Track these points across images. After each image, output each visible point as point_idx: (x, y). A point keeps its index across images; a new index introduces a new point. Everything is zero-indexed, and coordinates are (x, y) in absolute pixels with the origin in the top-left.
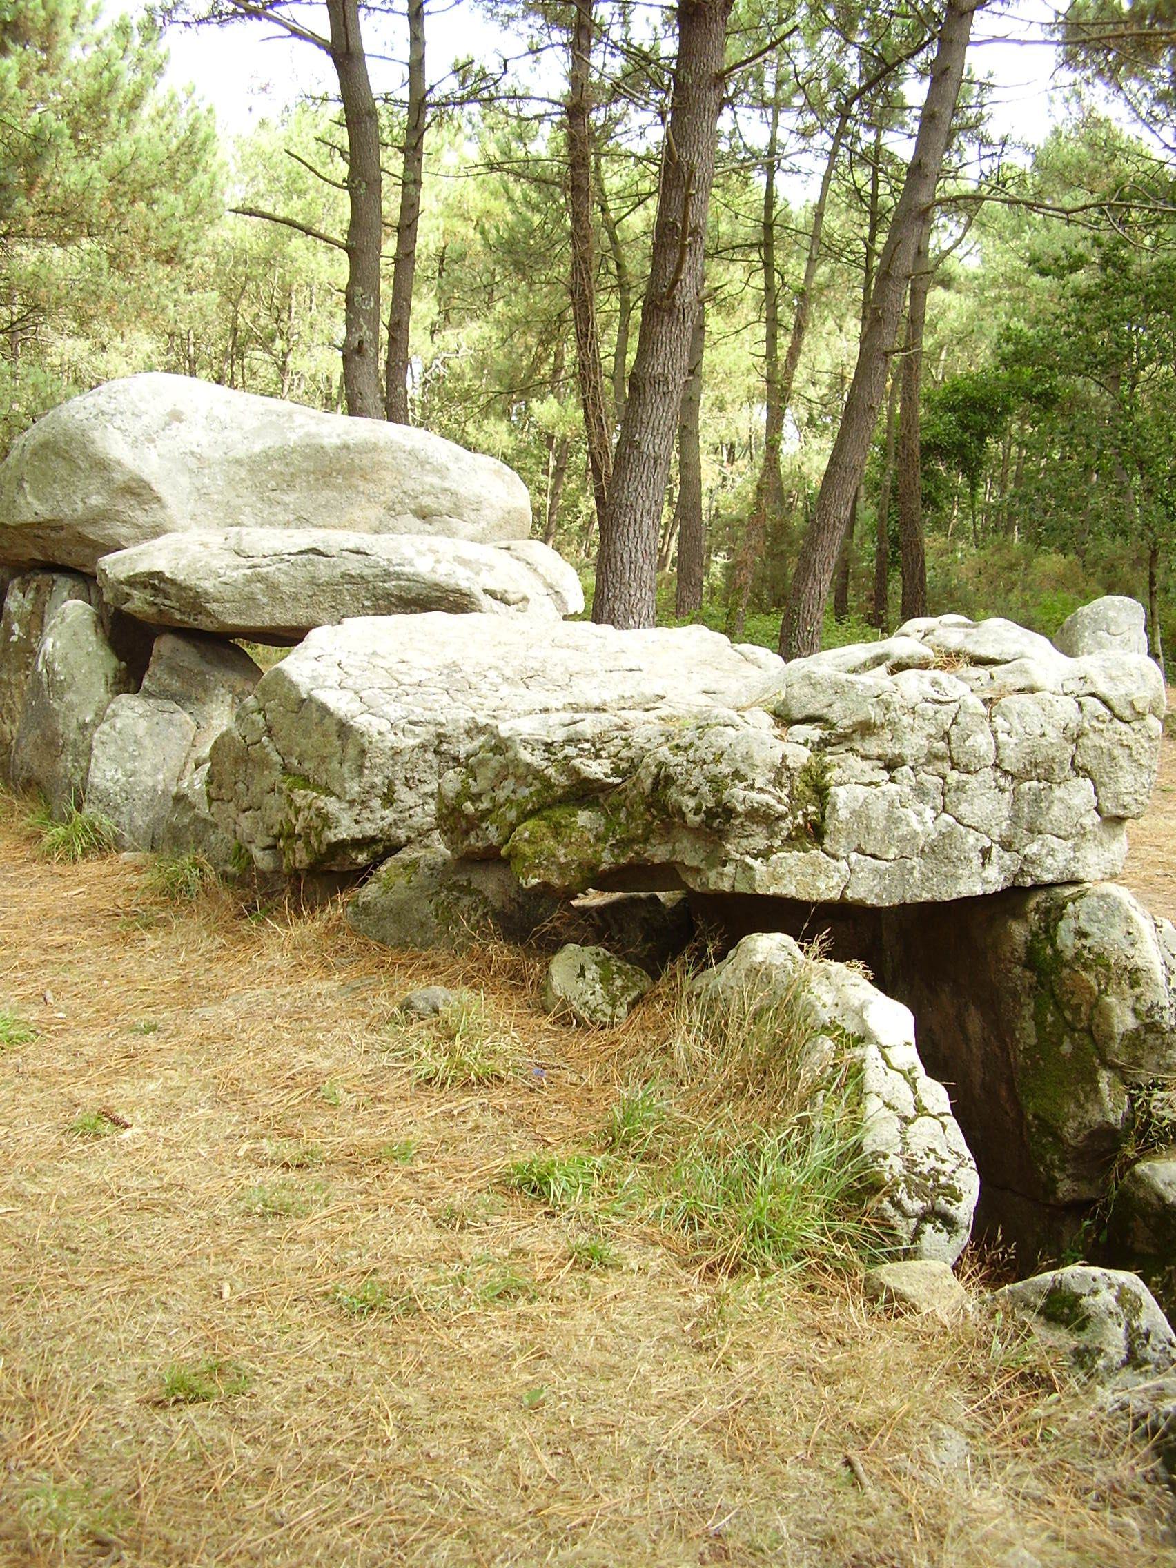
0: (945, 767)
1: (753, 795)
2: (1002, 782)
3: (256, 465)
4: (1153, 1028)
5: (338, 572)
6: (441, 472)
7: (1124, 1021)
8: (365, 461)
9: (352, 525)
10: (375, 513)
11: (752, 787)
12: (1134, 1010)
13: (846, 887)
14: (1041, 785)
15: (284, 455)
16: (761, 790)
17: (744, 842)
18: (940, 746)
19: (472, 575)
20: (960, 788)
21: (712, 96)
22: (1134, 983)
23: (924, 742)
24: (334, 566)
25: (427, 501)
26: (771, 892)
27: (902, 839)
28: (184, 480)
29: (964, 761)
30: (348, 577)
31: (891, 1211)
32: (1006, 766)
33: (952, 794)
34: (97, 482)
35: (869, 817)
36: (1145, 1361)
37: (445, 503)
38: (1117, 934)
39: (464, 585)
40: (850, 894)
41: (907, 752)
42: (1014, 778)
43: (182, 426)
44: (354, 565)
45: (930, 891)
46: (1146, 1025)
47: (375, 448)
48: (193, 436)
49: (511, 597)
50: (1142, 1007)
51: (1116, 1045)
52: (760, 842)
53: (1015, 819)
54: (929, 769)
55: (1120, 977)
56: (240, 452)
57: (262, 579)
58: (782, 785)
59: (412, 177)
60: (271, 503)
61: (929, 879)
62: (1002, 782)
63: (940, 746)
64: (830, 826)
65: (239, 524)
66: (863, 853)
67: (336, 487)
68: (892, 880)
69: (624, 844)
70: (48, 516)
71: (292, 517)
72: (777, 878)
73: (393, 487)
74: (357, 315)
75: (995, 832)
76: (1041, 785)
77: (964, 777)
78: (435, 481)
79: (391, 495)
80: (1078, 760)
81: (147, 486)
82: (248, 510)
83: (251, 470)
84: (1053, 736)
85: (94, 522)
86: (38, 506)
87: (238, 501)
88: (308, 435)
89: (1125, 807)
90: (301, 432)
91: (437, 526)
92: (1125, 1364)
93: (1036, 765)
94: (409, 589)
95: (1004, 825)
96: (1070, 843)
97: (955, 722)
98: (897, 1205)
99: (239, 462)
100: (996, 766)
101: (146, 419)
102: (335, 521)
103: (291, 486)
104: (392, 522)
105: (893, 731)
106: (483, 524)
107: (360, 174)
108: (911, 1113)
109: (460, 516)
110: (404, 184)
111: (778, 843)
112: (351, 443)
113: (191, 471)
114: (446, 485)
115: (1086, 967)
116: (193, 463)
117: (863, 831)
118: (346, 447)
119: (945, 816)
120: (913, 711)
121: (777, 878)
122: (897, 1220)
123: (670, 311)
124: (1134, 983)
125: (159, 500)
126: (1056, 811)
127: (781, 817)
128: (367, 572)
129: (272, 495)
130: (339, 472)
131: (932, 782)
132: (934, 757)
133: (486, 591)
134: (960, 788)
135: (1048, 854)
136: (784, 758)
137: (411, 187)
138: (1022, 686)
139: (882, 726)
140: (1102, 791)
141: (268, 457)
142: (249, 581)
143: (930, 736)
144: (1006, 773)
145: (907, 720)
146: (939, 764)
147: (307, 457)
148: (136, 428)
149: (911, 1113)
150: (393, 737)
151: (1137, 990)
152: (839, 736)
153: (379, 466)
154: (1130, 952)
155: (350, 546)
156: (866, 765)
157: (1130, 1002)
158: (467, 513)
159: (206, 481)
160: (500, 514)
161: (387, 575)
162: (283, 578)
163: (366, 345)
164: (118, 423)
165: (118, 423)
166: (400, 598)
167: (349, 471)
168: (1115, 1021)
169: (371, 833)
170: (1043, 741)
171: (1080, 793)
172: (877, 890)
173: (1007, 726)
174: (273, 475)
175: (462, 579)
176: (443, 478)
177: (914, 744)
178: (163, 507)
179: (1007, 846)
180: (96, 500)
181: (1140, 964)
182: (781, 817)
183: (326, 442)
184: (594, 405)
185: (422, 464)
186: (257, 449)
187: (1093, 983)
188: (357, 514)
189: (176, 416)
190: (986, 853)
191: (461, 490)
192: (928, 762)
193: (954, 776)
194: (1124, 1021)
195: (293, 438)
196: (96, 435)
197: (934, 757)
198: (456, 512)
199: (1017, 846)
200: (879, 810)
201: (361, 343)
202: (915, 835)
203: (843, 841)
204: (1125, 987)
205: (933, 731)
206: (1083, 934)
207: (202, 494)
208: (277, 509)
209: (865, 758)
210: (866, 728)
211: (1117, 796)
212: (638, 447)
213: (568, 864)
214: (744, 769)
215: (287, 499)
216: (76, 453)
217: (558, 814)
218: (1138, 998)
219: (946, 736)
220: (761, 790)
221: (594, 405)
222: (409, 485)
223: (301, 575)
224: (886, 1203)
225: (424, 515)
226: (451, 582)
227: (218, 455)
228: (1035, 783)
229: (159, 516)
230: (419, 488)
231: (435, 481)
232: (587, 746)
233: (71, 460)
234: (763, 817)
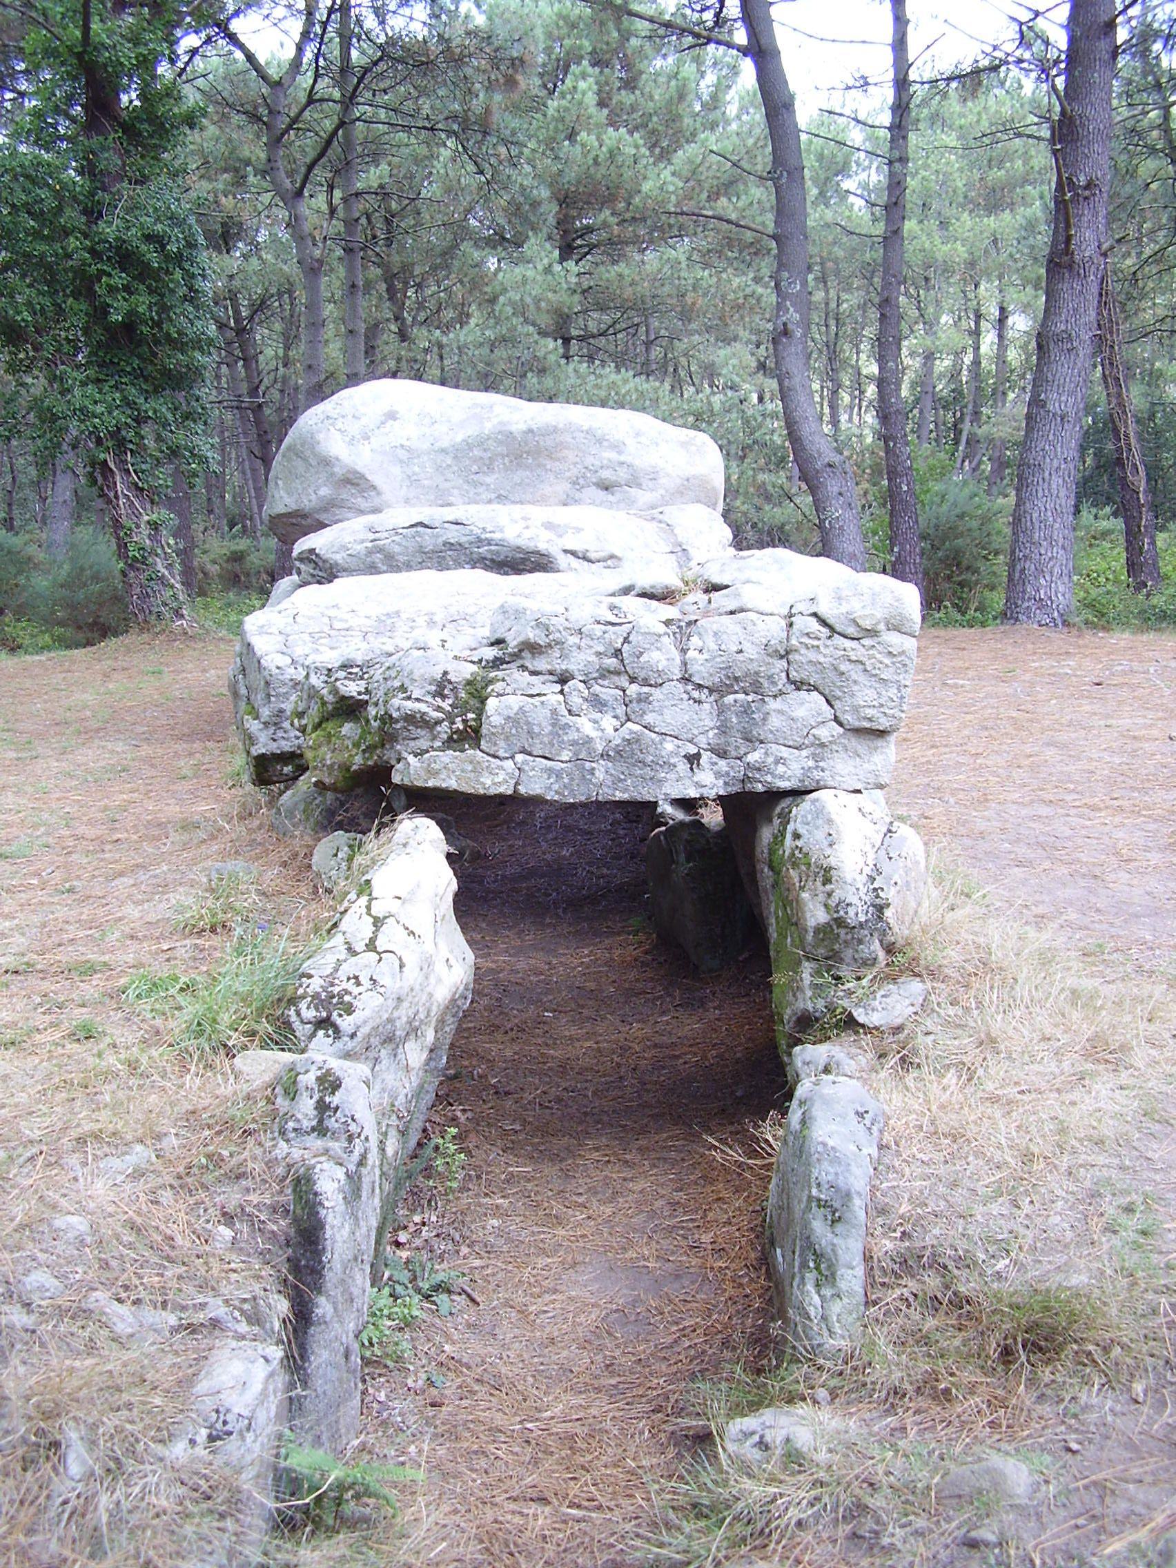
0: (623, 681)
1: (409, 705)
2: (696, 694)
3: (460, 452)
4: (840, 922)
5: (440, 540)
6: (618, 447)
7: (816, 915)
8: (549, 442)
9: (543, 501)
10: (563, 487)
11: (409, 698)
12: (826, 906)
13: (517, 784)
14: (750, 698)
15: (481, 442)
16: (418, 700)
17: (412, 743)
18: (612, 662)
19: (554, 537)
20: (643, 699)
21: (1103, 46)
22: (827, 881)
23: (593, 658)
24: (438, 536)
25: (606, 474)
26: (430, 784)
27: (574, 743)
28: (396, 470)
29: (642, 675)
30: (449, 545)
31: (294, 1018)
32: (696, 679)
33: (634, 704)
34: (323, 476)
35: (528, 723)
36: (327, 1129)
37: (623, 475)
38: (820, 835)
39: (542, 546)
40: (522, 790)
41: (572, 667)
42: (711, 691)
43: (396, 424)
44: (453, 534)
45: (625, 790)
46: (836, 920)
47: (555, 430)
48: (406, 432)
49: (592, 556)
50: (832, 903)
51: (810, 937)
52: (423, 744)
53: (723, 729)
54: (606, 683)
55: (816, 874)
56: (445, 443)
57: (380, 550)
58: (444, 697)
59: (897, 154)
60: (475, 484)
61: (620, 780)
62: (696, 694)
63: (612, 662)
64: (484, 731)
65: (449, 505)
66: (530, 754)
67: (528, 467)
68: (572, 779)
69: (370, 749)
70: (294, 507)
71: (493, 496)
72: (435, 774)
73: (575, 464)
74: (784, 299)
75: (702, 741)
76: (750, 698)
77: (646, 689)
78: (613, 455)
79: (575, 471)
80: (793, 674)
81: (362, 477)
82: (456, 492)
83: (456, 457)
84: (751, 652)
85: (326, 510)
86: (287, 500)
87: (447, 485)
88: (500, 423)
89: (870, 720)
90: (495, 421)
91: (618, 496)
92: (313, 1129)
93: (737, 679)
94: (498, 552)
95: (711, 734)
96: (804, 753)
97: (626, 640)
98: (298, 1014)
99: (443, 450)
100: (686, 680)
101: (364, 421)
102: (529, 497)
103: (490, 469)
104: (577, 495)
105: (561, 650)
106: (662, 492)
107: (782, 165)
108: (360, 946)
109: (639, 486)
110: (890, 163)
111: (438, 744)
112: (534, 427)
113: (401, 461)
114: (622, 458)
115: (795, 865)
116: (402, 454)
117: (524, 735)
118: (531, 431)
119: (629, 724)
120: (580, 632)
121: (435, 774)
122: (297, 1025)
123: (1070, 267)
124: (827, 881)
125: (374, 488)
126: (775, 722)
127: (438, 722)
128: (463, 539)
129: (476, 477)
130: (528, 453)
131: (607, 692)
132: (605, 673)
133: (566, 551)
134: (643, 699)
135: (777, 762)
136: (445, 673)
137: (897, 165)
138: (732, 608)
139: (550, 646)
140: (837, 704)
141: (468, 445)
142: (370, 552)
143: (598, 654)
144: (700, 686)
145: (573, 640)
146: (616, 678)
147: (500, 442)
148: (354, 428)
149: (360, 946)
150: (292, 671)
151: (828, 887)
152: (510, 655)
153: (561, 446)
154: (828, 852)
155: (450, 518)
156: (535, 679)
157: (821, 897)
158: (645, 483)
159: (416, 469)
160: (679, 481)
161: (480, 541)
162: (397, 549)
163: (790, 326)
164: (339, 425)
165: (339, 425)
166: (492, 560)
167: (537, 452)
168: (808, 915)
169: (287, 749)
170: (740, 657)
171: (808, 706)
172: (556, 787)
173: (700, 644)
174: (475, 460)
175: (543, 542)
176: (620, 453)
177: (580, 660)
178: (379, 494)
179: (722, 754)
180: (324, 491)
181: (833, 864)
182: (438, 722)
183: (514, 428)
184: (1111, 364)
185: (600, 441)
186: (459, 438)
187: (796, 880)
188: (547, 489)
189: (392, 416)
190: (693, 759)
191: (637, 462)
192: (603, 677)
193: (633, 689)
194: (816, 915)
195: (488, 427)
196: (320, 437)
197: (605, 673)
198: (634, 482)
199: (734, 754)
200: (540, 717)
201: (785, 324)
202: (589, 740)
203: (502, 744)
204: (818, 884)
205: (601, 649)
206: (797, 836)
207: (413, 481)
208: (481, 490)
209: (534, 673)
210: (532, 648)
211: (856, 709)
212: (1043, 406)
213: (332, 765)
214: (407, 683)
215: (488, 480)
216: (308, 453)
217: (330, 726)
218: (829, 895)
219: (618, 653)
220: (418, 700)
221: (1111, 364)
222: (589, 461)
223: (410, 544)
224: (292, 1012)
225: (606, 487)
226: (531, 545)
227: (425, 446)
228: (741, 696)
229: (377, 501)
230: (597, 463)
231: (613, 455)
232: (355, 670)
233: (305, 459)
234: (416, 721)
